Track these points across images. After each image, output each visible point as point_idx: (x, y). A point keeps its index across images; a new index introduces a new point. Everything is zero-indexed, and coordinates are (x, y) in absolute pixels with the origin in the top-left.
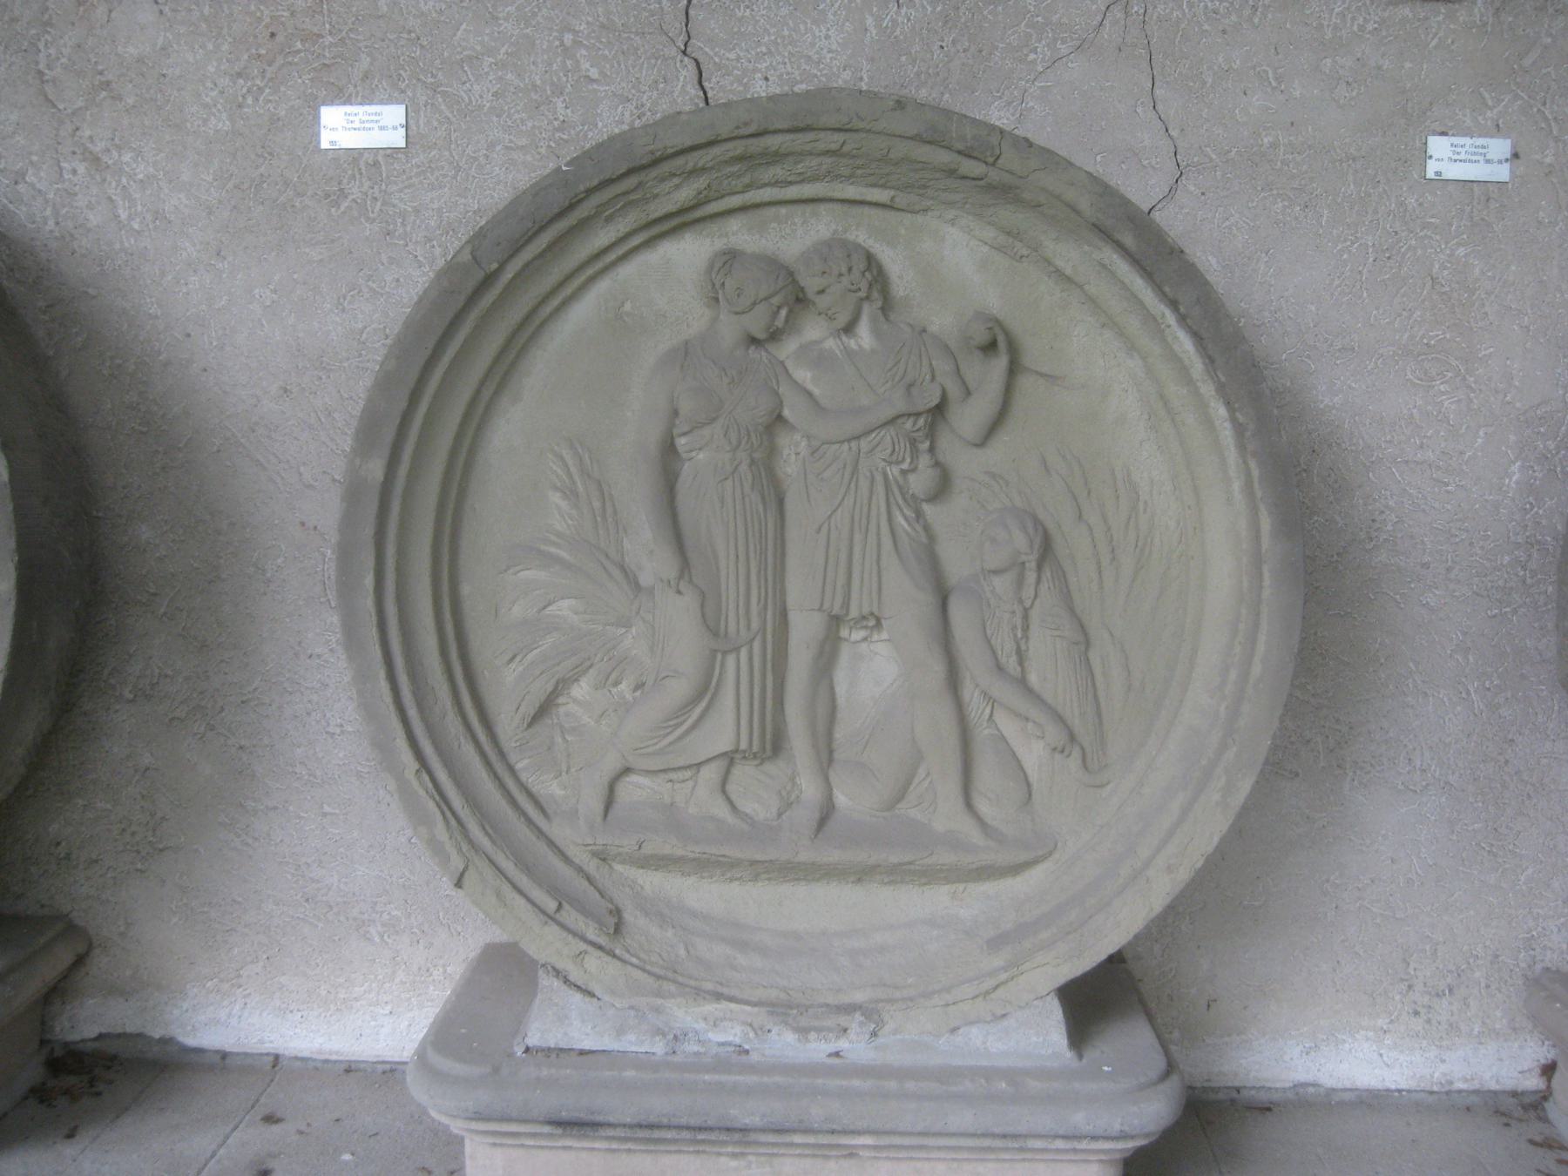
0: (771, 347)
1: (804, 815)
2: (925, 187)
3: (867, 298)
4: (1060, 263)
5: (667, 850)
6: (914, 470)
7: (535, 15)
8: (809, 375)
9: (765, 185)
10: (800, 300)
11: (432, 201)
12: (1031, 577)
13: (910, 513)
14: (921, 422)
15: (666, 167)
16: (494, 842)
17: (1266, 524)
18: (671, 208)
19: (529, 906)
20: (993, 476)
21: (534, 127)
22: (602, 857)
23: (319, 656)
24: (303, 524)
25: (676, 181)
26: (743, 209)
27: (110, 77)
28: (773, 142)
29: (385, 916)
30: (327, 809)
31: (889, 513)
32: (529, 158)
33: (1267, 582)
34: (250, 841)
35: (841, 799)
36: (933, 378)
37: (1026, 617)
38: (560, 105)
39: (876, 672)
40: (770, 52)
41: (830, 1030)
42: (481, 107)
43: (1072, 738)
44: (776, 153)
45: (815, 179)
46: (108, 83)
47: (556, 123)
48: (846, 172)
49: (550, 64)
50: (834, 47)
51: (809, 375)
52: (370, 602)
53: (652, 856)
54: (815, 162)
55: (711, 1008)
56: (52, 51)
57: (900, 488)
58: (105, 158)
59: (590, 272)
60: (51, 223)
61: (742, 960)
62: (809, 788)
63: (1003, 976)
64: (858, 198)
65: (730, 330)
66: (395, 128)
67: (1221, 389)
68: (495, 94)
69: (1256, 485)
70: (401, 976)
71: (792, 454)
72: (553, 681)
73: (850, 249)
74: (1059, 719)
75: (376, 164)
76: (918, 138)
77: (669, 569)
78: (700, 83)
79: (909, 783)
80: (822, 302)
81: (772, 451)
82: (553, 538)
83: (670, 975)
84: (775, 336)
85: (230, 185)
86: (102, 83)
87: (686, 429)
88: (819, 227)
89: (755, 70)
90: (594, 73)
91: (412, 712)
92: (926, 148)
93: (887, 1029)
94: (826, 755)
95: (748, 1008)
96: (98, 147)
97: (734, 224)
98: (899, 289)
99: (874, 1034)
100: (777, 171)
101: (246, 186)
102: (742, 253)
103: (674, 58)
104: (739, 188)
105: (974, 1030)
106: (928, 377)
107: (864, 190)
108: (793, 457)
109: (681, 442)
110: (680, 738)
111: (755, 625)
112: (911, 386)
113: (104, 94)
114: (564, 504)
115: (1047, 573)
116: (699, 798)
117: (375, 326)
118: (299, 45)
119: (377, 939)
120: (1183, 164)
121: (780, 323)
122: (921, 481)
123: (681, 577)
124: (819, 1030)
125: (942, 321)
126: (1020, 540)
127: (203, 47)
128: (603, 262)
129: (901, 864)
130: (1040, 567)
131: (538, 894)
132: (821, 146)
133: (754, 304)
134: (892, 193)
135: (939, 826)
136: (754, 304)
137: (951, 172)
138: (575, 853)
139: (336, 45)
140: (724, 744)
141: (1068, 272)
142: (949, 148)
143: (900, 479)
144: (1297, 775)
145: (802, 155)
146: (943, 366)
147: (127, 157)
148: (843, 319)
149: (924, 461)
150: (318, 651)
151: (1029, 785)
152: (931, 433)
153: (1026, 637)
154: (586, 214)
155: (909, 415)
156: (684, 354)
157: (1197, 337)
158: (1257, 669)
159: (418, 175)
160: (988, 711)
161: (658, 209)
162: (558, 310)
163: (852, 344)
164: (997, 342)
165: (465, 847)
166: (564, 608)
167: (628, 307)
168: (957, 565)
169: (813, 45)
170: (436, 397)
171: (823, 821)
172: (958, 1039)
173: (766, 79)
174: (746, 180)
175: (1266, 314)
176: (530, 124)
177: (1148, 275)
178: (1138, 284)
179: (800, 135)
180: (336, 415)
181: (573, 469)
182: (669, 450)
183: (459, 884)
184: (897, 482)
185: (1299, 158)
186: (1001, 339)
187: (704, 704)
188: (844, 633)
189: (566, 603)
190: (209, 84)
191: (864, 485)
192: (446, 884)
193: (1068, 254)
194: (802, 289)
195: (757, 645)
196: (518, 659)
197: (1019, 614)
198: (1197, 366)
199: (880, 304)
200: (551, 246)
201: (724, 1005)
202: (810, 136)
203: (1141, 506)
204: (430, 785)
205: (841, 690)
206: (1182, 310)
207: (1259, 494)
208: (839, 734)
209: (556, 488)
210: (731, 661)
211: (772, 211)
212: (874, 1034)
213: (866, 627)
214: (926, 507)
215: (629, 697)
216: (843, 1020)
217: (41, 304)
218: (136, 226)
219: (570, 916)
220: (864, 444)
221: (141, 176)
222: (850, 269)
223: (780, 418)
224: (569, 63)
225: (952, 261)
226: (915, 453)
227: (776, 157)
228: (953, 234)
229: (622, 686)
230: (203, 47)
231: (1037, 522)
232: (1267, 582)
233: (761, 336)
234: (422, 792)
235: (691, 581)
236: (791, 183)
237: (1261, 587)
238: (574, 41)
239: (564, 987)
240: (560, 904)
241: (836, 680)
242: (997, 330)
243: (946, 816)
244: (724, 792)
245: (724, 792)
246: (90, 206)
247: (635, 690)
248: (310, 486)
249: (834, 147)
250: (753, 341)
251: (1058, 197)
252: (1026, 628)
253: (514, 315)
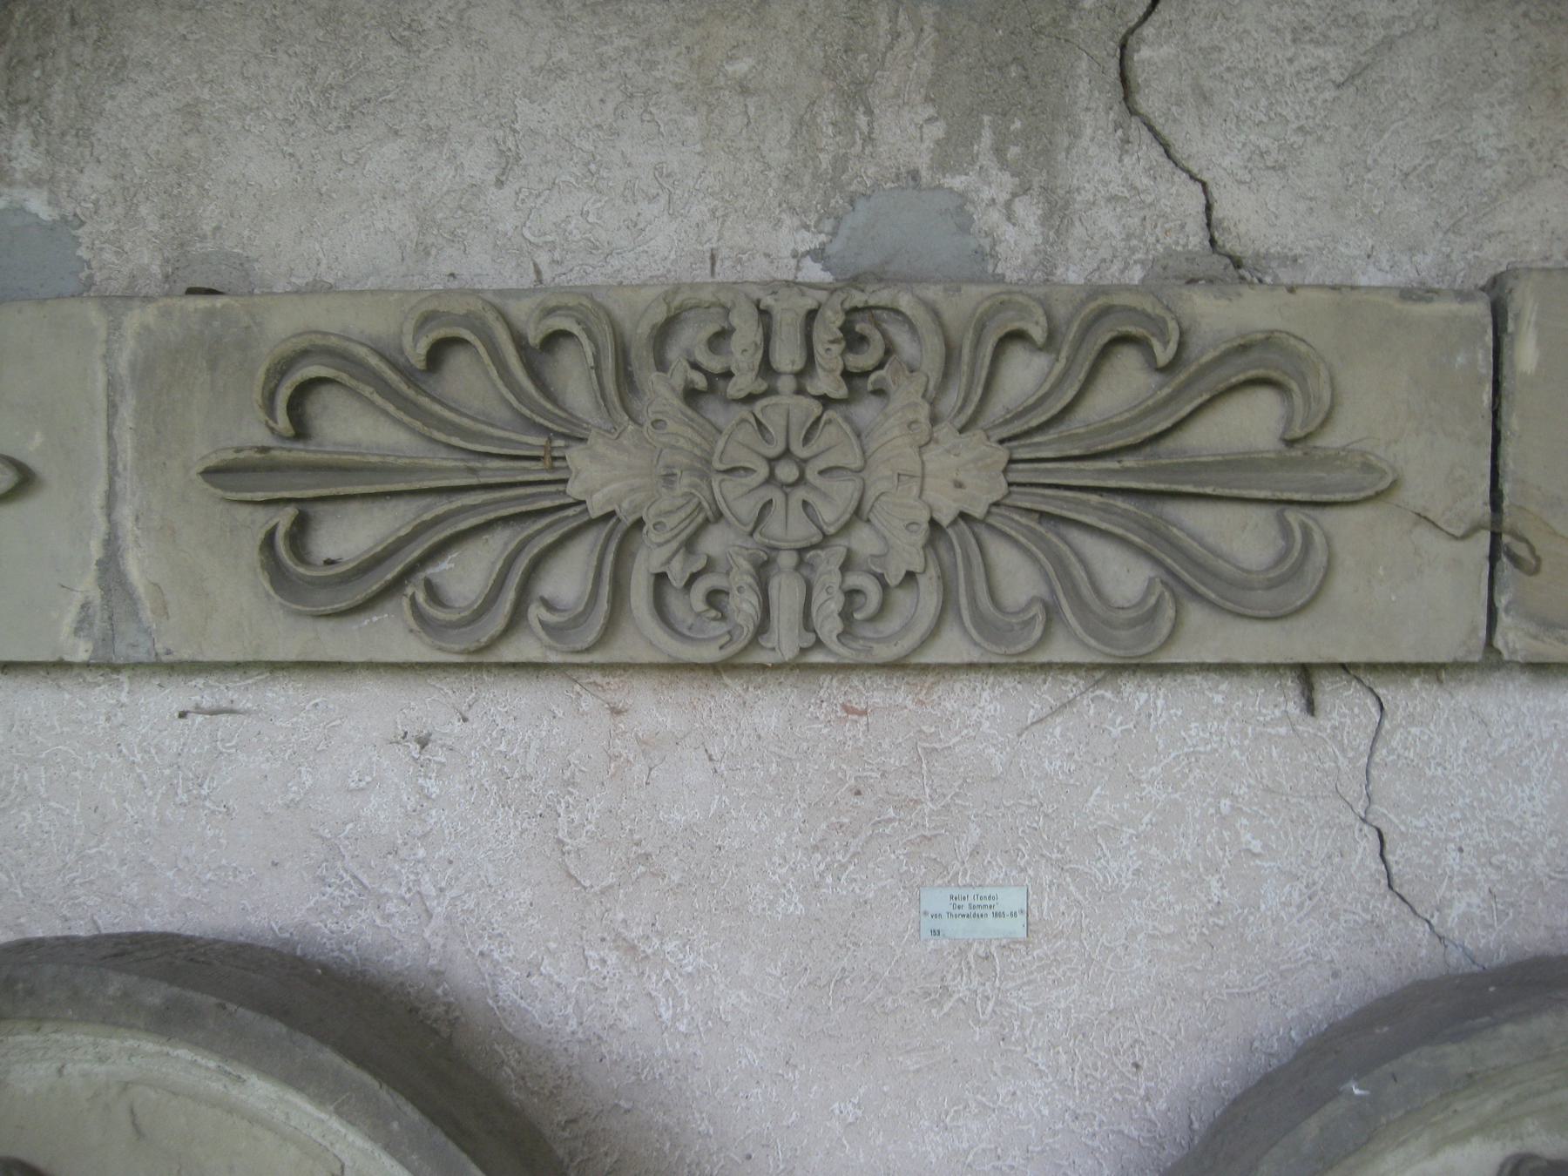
7: (1185, 776)
11: (1058, 999)
21: (1183, 911)
27: (649, 849)
32: (1177, 948)
38: (1214, 883)
40: (1464, 819)
46: (647, 856)
49: (1204, 836)
50: (1539, 809)
56: (576, 816)
58: (642, 947)
60: (573, 1022)
66: (1013, 914)
68: (1137, 872)
75: (988, 957)
85: (804, 981)
86: (639, 856)
89: (1448, 840)
90: (1256, 846)
96: (635, 933)
101: (823, 982)
103: (1351, 827)
113: (642, 869)
117: (984, 1145)
118: (891, 812)
127: (769, 814)
139: (939, 813)
147: (670, 946)
159: (1041, 968)
169: (1514, 807)
173: (1461, 850)
176: (1178, 908)
190: (776, 859)
217: (561, 1118)
218: (682, 1028)
221: (689, 969)
224: (1226, 834)
230: (769, 814)
238: (1232, 807)
246: (623, 1004)
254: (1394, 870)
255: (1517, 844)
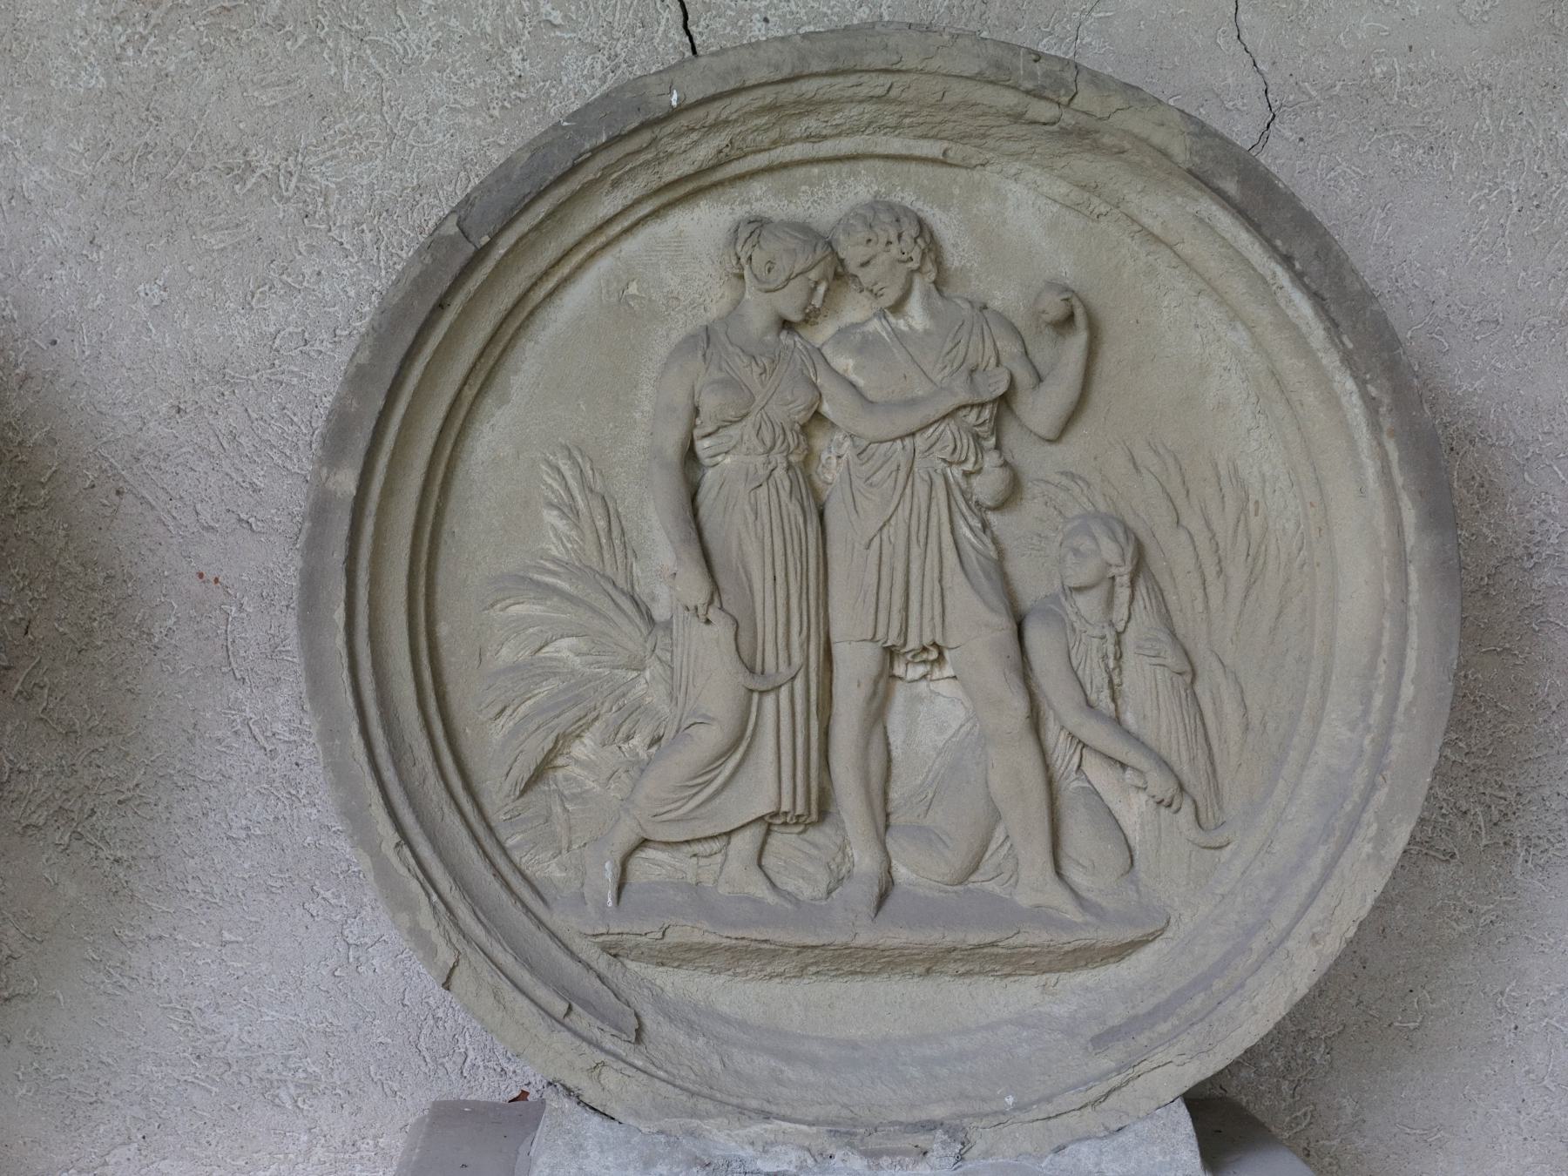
0: (806, 332)
1: (861, 892)
2: (984, 136)
3: (919, 270)
4: (1146, 220)
5: (696, 937)
6: (979, 471)
8: (851, 363)
9: (792, 142)
10: (840, 275)
12: (1123, 594)
13: (977, 524)
14: (986, 414)
15: (683, 121)
16: (488, 931)
17: (1410, 515)
18: (687, 169)
19: (534, 1009)
20: (1072, 476)
21: (484, 84)
22: (614, 952)
23: (219, 741)
24: (201, 575)
25: (694, 136)
26: (769, 169)
28: (809, 87)
29: (301, 1075)
30: (227, 936)
31: (951, 521)
32: (479, 122)
33: (1414, 584)
34: (125, 982)
35: (901, 872)
36: (998, 364)
37: (1118, 643)
38: (516, 57)
39: (938, 715)
41: (905, 1153)
42: (420, 60)
43: (1181, 788)
44: (810, 102)
45: (852, 132)
47: (511, 79)
48: (891, 120)
51: (851, 363)
52: (340, 640)
53: (678, 945)
54: (855, 111)
55: (757, 1129)
57: (963, 493)
59: (590, 247)
61: (789, 1073)
62: (864, 860)
63: (1116, 1080)
64: (904, 152)
65: (758, 313)
67: (1347, 359)
68: (437, 44)
69: (1396, 471)
70: (319, 1152)
71: (833, 459)
72: (552, 737)
73: (898, 214)
74: (1164, 764)
76: (978, 78)
77: (694, 588)
78: (685, 26)
79: (985, 848)
80: (866, 276)
81: (809, 457)
82: (549, 565)
83: (705, 1091)
84: (811, 317)
87: (709, 430)
88: (860, 187)
89: (753, 10)
91: (389, 774)
92: (989, 90)
93: (975, 1151)
94: (883, 823)
95: (804, 1128)
97: (758, 187)
98: (953, 260)
99: (960, 1158)
100: (812, 124)
102: (769, 221)
104: (766, 145)
105: (1084, 1148)
106: (993, 361)
107: (912, 142)
108: (834, 461)
109: (703, 446)
110: (717, 793)
111: (797, 659)
112: (972, 371)
114: (561, 525)
115: (1141, 589)
116: (732, 870)
119: (289, 1106)
120: (1275, 105)
121: (817, 302)
122: (988, 485)
123: (711, 602)
124: (892, 1153)
125: (1005, 297)
126: (1110, 550)
128: (605, 236)
129: (980, 946)
130: (1133, 584)
131: (542, 994)
132: (864, 91)
133: (788, 280)
134: (946, 144)
135: (1024, 899)
136: (788, 280)
137: (1017, 117)
138: (579, 945)
140: (763, 807)
141: (1157, 230)
142: (1015, 88)
143: (964, 485)
144: (1453, 856)
145: (835, 103)
146: (1009, 348)
148: (891, 296)
149: (991, 460)
150: (219, 734)
151: (1130, 849)
152: (997, 430)
153: (1119, 667)
154: (591, 177)
155: (972, 406)
156: (706, 339)
157: (1316, 297)
158: (1408, 691)
159: (343, 143)
160: (1076, 760)
161: (671, 172)
162: (551, 294)
163: (901, 324)
164: (1073, 317)
165: (454, 936)
166: (563, 648)
167: (633, 289)
168: (1032, 586)
170: (415, 394)
171: (883, 898)
172: (1064, 1160)
173: (766, 20)
174: (774, 134)
175: (1385, 283)
176: (479, 81)
177: (1254, 226)
178: (1244, 239)
179: (840, 79)
180: (243, 440)
181: (572, 483)
182: (690, 455)
183: (447, 985)
184: (958, 484)
185: (1420, 90)
186: (1079, 312)
187: (738, 756)
188: (899, 670)
189: (565, 643)
191: (922, 489)
192: (429, 982)
193: (1164, 208)
194: (841, 261)
195: (799, 684)
196: (508, 712)
197: (1111, 639)
198: (1317, 334)
199: (933, 276)
200: (550, 215)
201: (776, 1125)
202: (853, 79)
203: (1251, 506)
204: (412, 861)
205: (896, 740)
206: (1298, 266)
207: (1399, 480)
208: (894, 795)
209: (551, 505)
210: (769, 701)
211: (800, 172)
212: (960, 1158)
213: (924, 662)
214: (992, 517)
215: (643, 755)
216: (922, 1140)
219: (583, 1020)
220: (920, 441)
222: (900, 236)
223: (818, 416)
225: (1018, 220)
226: (980, 450)
227: (810, 106)
228: (1015, 190)
229: (634, 742)
231: (1127, 530)
232: (1414, 584)
233: (795, 317)
234: (403, 871)
235: (721, 608)
236: (825, 137)
237: (1407, 592)
239: (579, 1108)
240: (570, 1008)
241: (890, 728)
242: (1075, 301)
243: (1032, 885)
244: (760, 866)
245: (760, 866)
247: (650, 746)
248: (210, 528)
249: (880, 91)
250: (786, 325)
251: (1145, 141)
252: (1119, 657)
253: (505, 300)
254: (697, 42)
255: (825, 15)
